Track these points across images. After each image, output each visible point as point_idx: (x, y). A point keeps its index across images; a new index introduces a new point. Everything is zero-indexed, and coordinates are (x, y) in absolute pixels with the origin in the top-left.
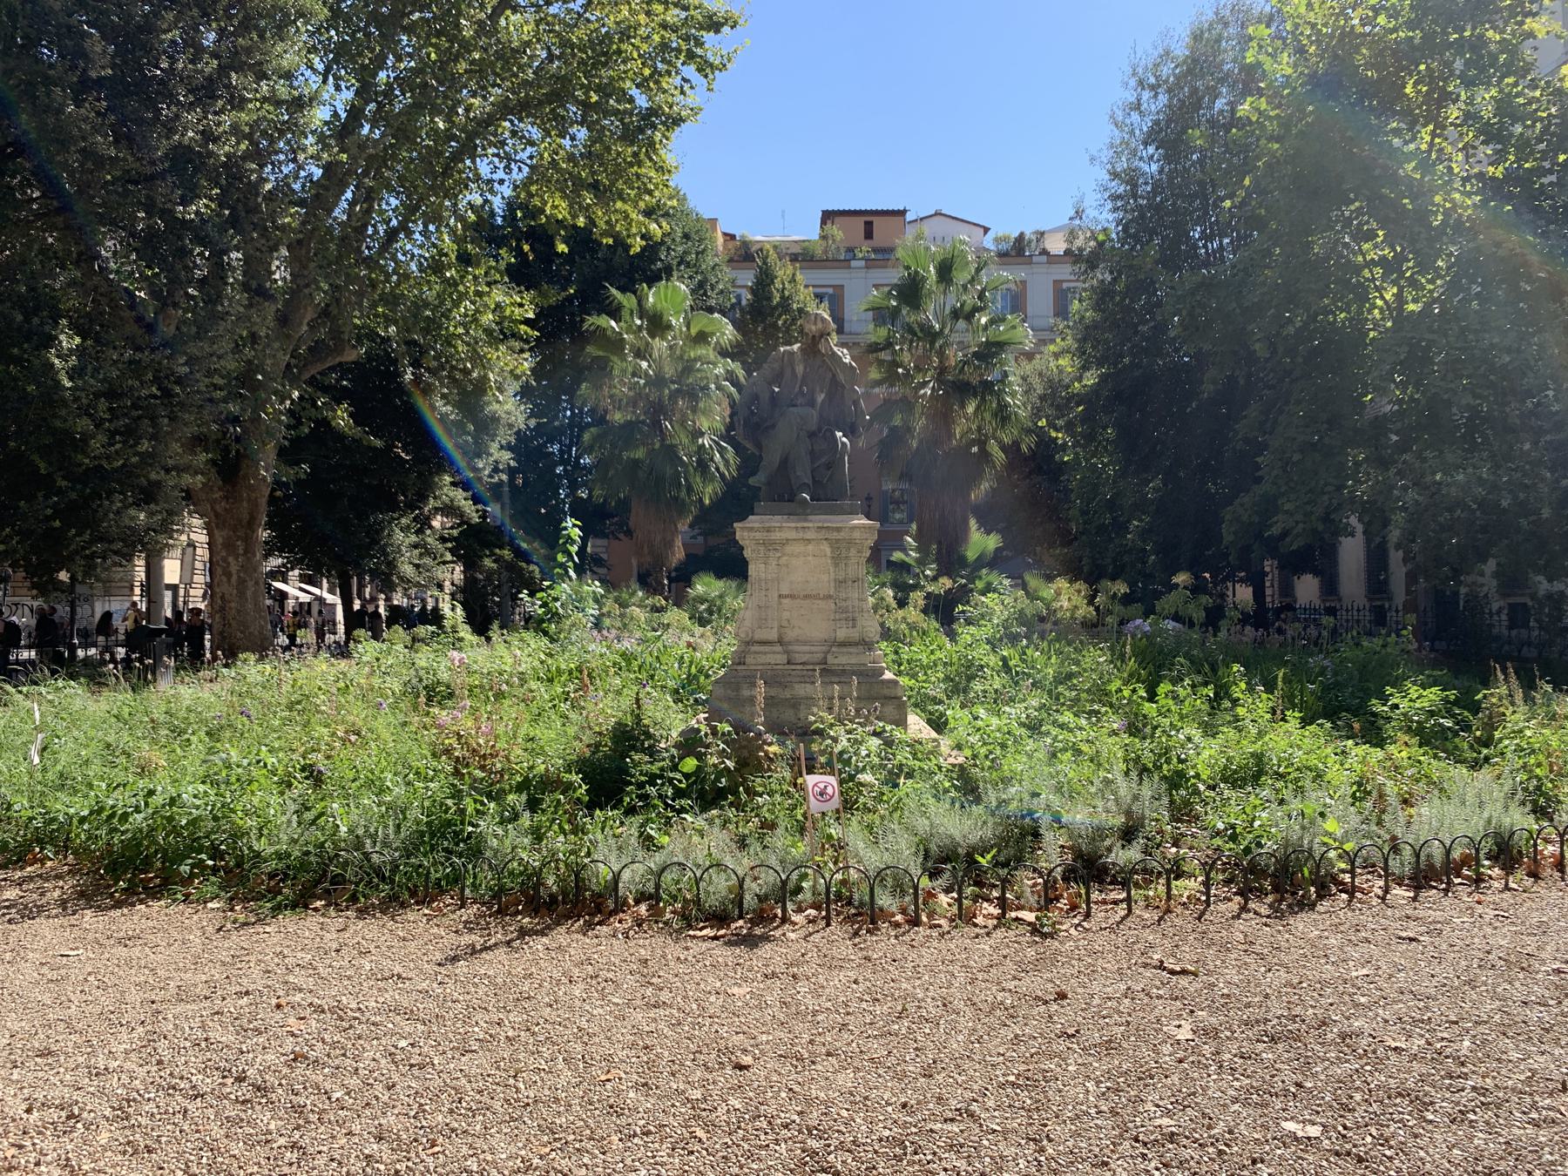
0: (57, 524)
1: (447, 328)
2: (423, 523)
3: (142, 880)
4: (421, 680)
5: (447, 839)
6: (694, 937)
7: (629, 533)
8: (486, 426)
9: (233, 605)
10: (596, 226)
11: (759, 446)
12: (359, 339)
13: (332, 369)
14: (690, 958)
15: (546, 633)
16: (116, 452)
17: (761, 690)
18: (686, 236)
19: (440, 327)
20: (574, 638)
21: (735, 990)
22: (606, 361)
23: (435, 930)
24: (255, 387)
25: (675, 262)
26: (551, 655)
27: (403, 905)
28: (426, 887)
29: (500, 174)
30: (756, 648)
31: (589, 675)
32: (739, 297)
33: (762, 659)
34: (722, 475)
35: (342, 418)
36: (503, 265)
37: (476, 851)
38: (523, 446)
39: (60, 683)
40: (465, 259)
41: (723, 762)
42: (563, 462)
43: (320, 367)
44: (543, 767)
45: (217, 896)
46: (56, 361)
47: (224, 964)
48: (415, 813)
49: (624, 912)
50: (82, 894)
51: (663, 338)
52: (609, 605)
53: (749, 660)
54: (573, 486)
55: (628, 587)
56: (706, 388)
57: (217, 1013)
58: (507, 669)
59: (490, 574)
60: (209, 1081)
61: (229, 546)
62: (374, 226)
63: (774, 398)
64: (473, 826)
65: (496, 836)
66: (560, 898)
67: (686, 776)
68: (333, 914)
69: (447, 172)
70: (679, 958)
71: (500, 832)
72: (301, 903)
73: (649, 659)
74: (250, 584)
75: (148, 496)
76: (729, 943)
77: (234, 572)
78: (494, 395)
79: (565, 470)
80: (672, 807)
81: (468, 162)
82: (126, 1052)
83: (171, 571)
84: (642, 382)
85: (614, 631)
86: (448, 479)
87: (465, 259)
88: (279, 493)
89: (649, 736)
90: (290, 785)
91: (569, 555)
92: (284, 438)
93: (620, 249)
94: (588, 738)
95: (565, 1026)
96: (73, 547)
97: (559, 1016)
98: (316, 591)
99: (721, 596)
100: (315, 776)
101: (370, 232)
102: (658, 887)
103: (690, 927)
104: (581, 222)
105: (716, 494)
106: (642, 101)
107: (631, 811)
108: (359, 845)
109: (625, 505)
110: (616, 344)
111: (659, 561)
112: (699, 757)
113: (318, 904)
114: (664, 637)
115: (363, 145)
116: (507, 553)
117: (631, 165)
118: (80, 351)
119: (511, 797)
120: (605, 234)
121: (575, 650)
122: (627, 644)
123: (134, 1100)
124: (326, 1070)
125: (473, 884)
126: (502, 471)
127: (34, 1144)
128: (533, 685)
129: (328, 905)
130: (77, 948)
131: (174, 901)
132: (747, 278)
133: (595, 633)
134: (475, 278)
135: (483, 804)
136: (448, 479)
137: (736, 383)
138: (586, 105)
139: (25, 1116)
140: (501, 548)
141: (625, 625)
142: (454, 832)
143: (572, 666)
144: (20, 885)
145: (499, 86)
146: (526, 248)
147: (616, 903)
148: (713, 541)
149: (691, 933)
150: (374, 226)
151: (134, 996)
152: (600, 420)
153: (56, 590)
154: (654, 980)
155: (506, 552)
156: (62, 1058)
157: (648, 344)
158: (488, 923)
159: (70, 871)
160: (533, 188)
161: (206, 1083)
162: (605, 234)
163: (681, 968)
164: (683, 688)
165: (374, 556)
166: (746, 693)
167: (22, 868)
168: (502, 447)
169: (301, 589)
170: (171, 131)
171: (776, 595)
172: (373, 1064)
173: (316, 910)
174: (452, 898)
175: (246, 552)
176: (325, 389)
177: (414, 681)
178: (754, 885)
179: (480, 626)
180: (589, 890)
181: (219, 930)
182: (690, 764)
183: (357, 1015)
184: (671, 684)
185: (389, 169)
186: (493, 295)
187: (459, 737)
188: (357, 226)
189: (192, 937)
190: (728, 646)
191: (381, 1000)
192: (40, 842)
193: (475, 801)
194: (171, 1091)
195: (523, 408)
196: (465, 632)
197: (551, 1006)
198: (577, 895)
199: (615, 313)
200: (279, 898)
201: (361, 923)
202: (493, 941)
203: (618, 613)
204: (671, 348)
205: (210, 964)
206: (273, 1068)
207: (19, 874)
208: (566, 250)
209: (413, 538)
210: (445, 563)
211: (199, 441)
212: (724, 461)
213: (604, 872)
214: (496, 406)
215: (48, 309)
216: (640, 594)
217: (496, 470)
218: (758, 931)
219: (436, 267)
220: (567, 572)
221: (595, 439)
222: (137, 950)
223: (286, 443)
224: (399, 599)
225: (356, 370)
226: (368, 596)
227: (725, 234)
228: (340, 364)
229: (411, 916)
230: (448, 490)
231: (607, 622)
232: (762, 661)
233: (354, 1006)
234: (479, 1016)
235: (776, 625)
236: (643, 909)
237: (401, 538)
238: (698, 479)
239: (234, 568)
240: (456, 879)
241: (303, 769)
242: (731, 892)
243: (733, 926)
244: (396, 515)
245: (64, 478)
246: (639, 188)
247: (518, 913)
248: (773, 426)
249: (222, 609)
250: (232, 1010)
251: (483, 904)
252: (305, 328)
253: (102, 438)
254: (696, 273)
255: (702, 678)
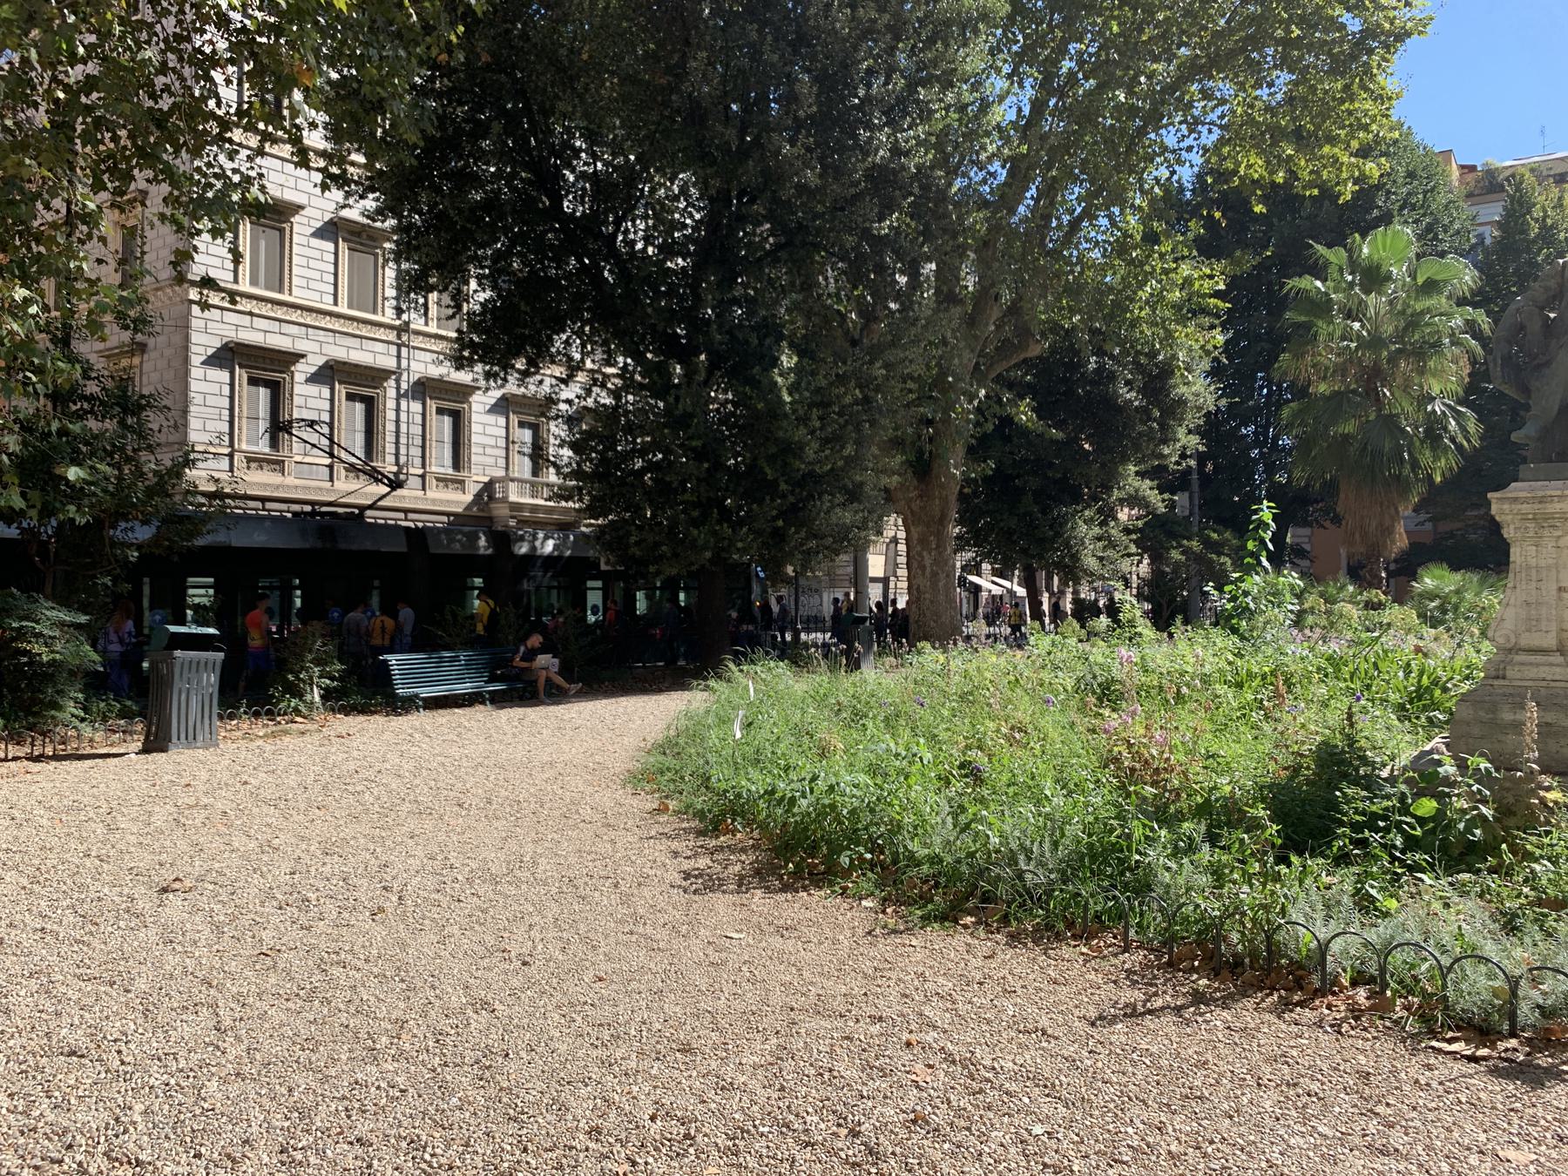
0: (780, 523)
1: (1132, 311)
2: (1108, 515)
3: (809, 864)
4: (1095, 677)
5: (1110, 865)
6: (1439, 1051)
7: (1337, 520)
8: (1174, 409)
9: (927, 596)
10: (1298, 179)
11: (1526, 391)
12: (1043, 334)
13: (1017, 366)
14: (1434, 1084)
15: (1234, 631)
16: (826, 457)
17: (1532, 713)
18: (1411, 175)
19: (1127, 310)
20: (1269, 637)
21: (1510, 1153)
22: (1307, 327)
23: (1092, 976)
24: (946, 389)
25: (1396, 207)
26: (1239, 655)
27: (1059, 937)
28: (1085, 918)
29: (1189, 142)
30: (1522, 658)
31: (1286, 681)
32: (1481, 237)
33: (1532, 673)
34: (1459, 447)
35: (1025, 414)
36: (1191, 235)
37: (1143, 888)
38: (1212, 427)
39: (772, 664)
40: (1151, 238)
41: (1476, 808)
42: (1257, 444)
43: (1005, 365)
44: (1228, 789)
45: (872, 894)
46: (779, 380)
47: (865, 976)
48: (1074, 830)
49: (1334, 994)
50: (758, 872)
51: (1379, 293)
52: (1312, 600)
53: (1509, 673)
54: (1271, 470)
55: (1336, 580)
56: (1437, 345)
57: (847, 1038)
58: (1189, 669)
59: (1177, 566)
60: (823, 1126)
61: (923, 541)
62: (1058, 219)
63: (1548, 325)
64: (1140, 854)
65: (1168, 869)
66: (1247, 960)
67: (1421, 821)
68: (983, 936)
69: (1130, 150)
70: (1417, 1081)
71: (1174, 866)
72: (949, 917)
73: (1364, 666)
74: (942, 576)
75: (854, 495)
76: (1495, 1072)
77: (928, 565)
78: (1182, 375)
79: (1261, 453)
80: (1401, 861)
81: (1153, 136)
82: (755, 1067)
83: (876, 565)
84: (1353, 345)
85: (1318, 630)
86: (1132, 468)
87: (1151, 238)
88: (966, 490)
89: (1364, 760)
90: (948, 783)
91: (1262, 542)
92: (972, 436)
93: (1327, 203)
94: (1284, 758)
95: (1249, 1154)
96: (793, 544)
97: (1241, 1136)
98: (1007, 584)
99: (1457, 592)
100: (972, 773)
101: (1054, 225)
102: (1383, 970)
103: (1433, 1034)
104: (1280, 177)
105: (1451, 469)
106: (1354, 25)
107: (1342, 859)
108: (1013, 861)
109: (1331, 488)
110: (1321, 306)
111: (1375, 551)
112: (1440, 797)
113: (969, 920)
114: (1383, 639)
115: (1044, 138)
116: (1195, 545)
117: (1342, 101)
118: (798, 369)
119: (1187, 826)
120: (1311, 185)
121: (1270, 651)
122: (1334, 647)
123: (748, 1132)
124: (946, 1146)
125: (1139, 925)
126: (1190, 456)
127: (646, 1163)
128: (1221, 689)
129: (978, 923)
130: (741, 931)
131: (833, 892)
132: (1493, 212)
133: (1295, 632)
134: (1162, 256)
135: (1152, 829)
136: (1132, 468)
137: (1477, 334)
138: (1287, 43)
139: (648, 1123)
140: (1189, 539)
141: (1332, 624)
142: (1118, 858)
143: (1266, 669)
144: (712, 854)
145: (1186, 45)
146: (1217, 215)
147: (1323, 980)
148: (1445, 527)
149: (1434, 1043)
150: (1058, 219)
151: (777, 998)
152: (1301, 392)
153: (782, 581)
154: (1380, 1109)
155: (1195, 543)
156: (699, 1058)
157: (1361, 301)
158: (1155, 977)
159: (753, 845)
160: (1226, 150)
161: (821, 1128)
162: (1311, 185)
163: (1421, 1098)
164: (1411, 702)
165: (1057, 549)
166: (1507, 716)
167: (717, 837)
168: (1190, 432)
169: (993, 582)
170: (866, 154)
171: (1555, 587)
172: (1000, 1150)
173: (965, 927)
174: (1115, 937)
175: (938, 546)
176: (1010, 386)
177: (1089, 677)
178: (1534, 994)
179: (1162, 620)
180: (1286, 956)
181: (869, 933)
182: (1427, 806)
183: (990, 1075)
184: (1394, 697)
185: (1071, 156)
186: (1179, 270)
187: (1130, 745)
188: (1042, 216)
189: (841, 937)
190: (1480, 654)
191: (1020, 1060)
192: (734, 814)
193: (1145, 826)
194: (784, 1130)
195: (1212, 388)
196: (1146, 630)
197: (1231, 1117)
198: (1269, 959)
199: (1319, 271)
200: (930, 907)
201: (1010, 952)
202: (1159, 1003)
203: (1323, 608)
204: (1391, 303)
205: (853, 974)
206: (890, 1127)
207: (714, 843)
208: (1264, 211)
209: (1097, 530)
210: (1129, 555)
211: (897, 443)
212: (1465, 428)
213: (1307, 940)
214: (1182, 389)
215: (771, 331)
216: (1351, 588)
217: (1183, 456)
218: (1543, 1061)
219: (1121, 248)
220: (1259, 563)
221: (1295, 415)
222: (791, 942)
223: (973, 441)
224: (1086, 594)
225: (1041, 365)
226: (1056, 590)
227: (1463, 167)
228: (1025, 361)
229: (1066, 951)
230: (1132, 480)
231: (1310, 619)
232: (1532, 675)
233: (988, 1062)
234: (1136, 1110)
235: (1554, 627)
236: (1361, 994)
237: (1084, 530)
238: (1427, 453)
239: (928, 562)
240: (1120, 915)
241: (962, 766)
242: (1496, 995)
243: (1501, 1045)
244: (1079, 508)
245: (786, 482)
246: (1351, 125)
247: (1193, 970)
248: (1547, 364)
249: (918, 599)
250: (862, 1037)
251: (1152, 950)
252: (992, 328)
253: (815, 445)
254: (1424, 215)
255: (1437, 692)
